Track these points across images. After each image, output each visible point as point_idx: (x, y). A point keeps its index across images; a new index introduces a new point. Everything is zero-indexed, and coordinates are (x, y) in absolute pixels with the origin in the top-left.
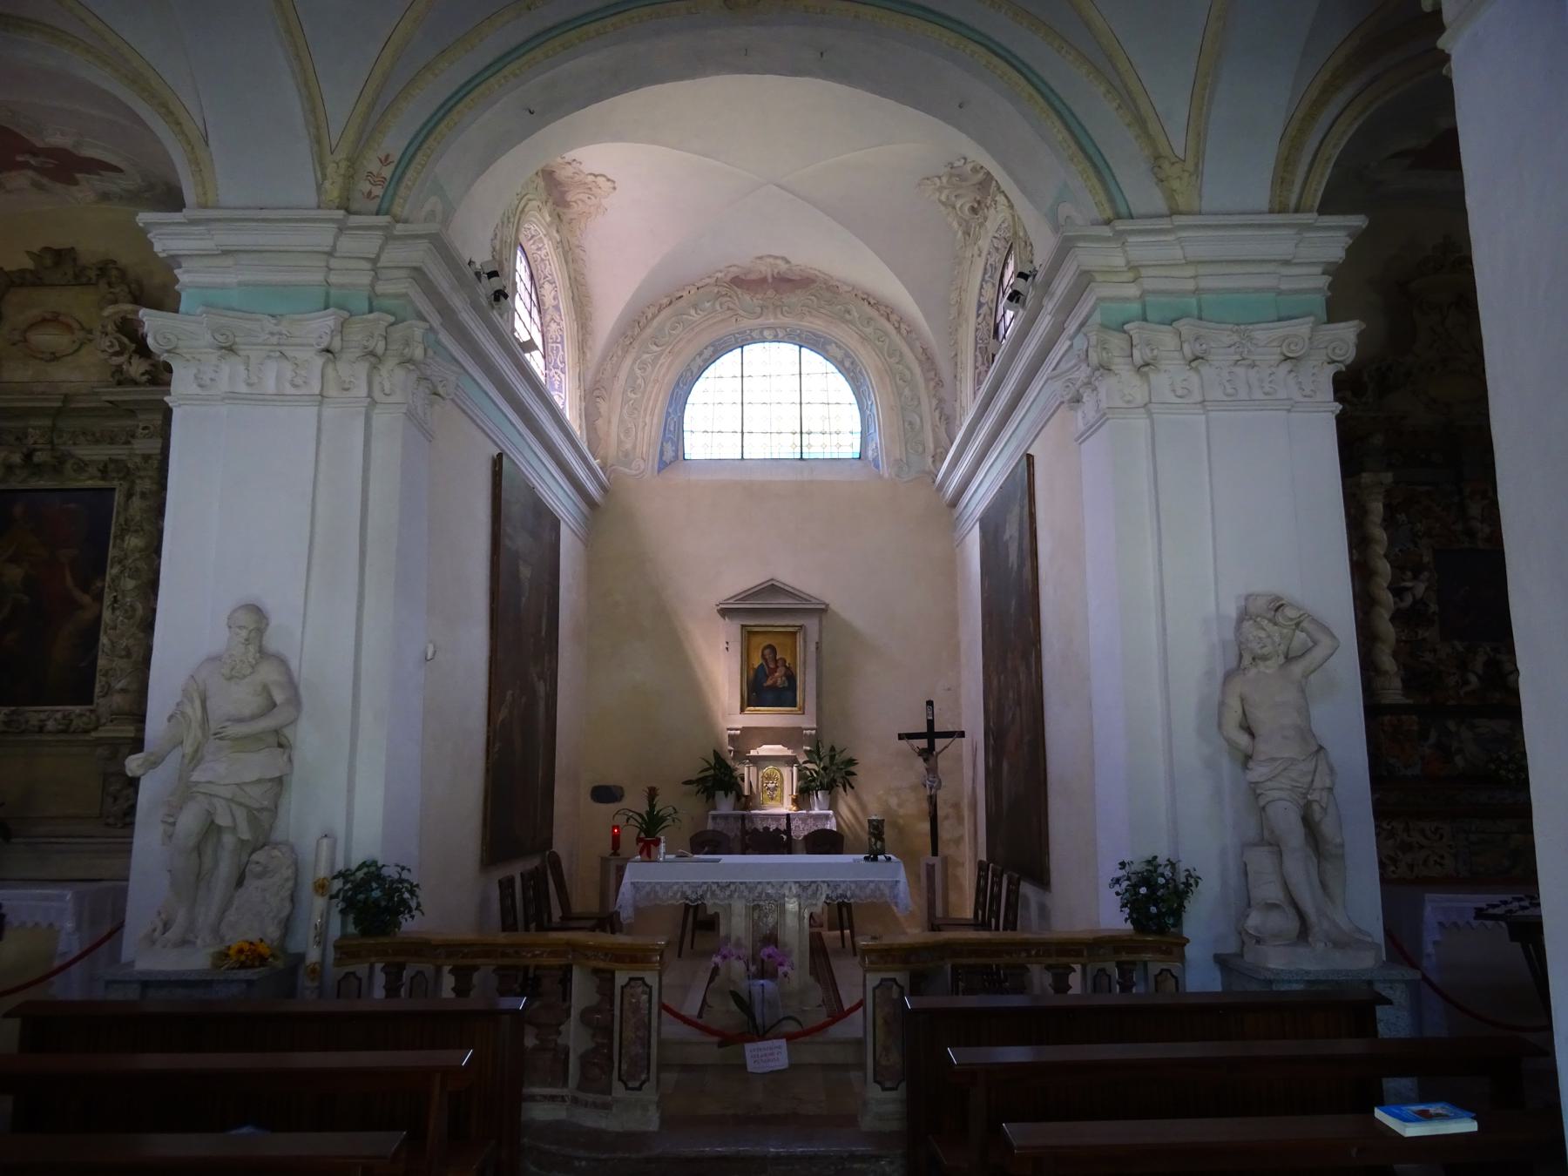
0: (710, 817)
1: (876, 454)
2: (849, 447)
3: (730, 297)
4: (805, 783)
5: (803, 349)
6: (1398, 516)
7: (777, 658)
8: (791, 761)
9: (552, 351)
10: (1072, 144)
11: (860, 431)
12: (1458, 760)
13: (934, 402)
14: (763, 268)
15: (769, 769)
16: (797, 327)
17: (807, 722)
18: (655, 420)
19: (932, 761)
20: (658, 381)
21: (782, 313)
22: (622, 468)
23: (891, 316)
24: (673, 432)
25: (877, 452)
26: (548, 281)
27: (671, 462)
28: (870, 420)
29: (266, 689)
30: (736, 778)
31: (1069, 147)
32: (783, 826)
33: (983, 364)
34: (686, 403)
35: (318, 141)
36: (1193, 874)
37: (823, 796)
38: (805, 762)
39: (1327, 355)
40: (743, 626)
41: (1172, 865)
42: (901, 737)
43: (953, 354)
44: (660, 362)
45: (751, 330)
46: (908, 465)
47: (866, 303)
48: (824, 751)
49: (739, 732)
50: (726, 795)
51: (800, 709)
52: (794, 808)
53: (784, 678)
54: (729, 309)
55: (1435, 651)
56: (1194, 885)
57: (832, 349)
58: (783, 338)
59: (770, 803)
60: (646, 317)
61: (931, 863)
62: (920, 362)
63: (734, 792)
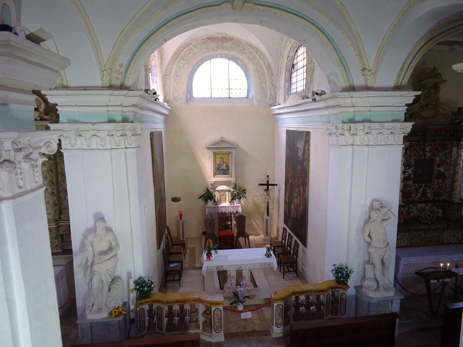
1: (252, 97)
2: (244, 94)
3: (207, 43)
6: (407, 151)
7: (224, 161)
10: (339, 60)
12: (412, 214)
13: (270, 81)
17: (232, 179)
18: (184, 86)
19: (268, 192)
20: (185, 73)
21: (224, 50)
22: (175, 102)
23: (258, 51)
24: (190, 89)
25: (253, 96)
27: (189, 99)
28: (250, 86)
29: (109, 241)
31: (338, 62)
35: (100, 63)
36: (352, 271)
37: (237, 200)
39: (403, 131)
40: (214, 152)
41: (347, 267)
43: (278, 67)
44: (185, 67)
45: (213, 55)
46: (262, 101)
47: (250, 47)
48: (238, 188)
49: (213, 183)
51: (230, 176)
53: (226, 167)
55: (411, 187)
56: (352, 273)
57: (239, 61)
58: (223, 57)
61: (267, 219)
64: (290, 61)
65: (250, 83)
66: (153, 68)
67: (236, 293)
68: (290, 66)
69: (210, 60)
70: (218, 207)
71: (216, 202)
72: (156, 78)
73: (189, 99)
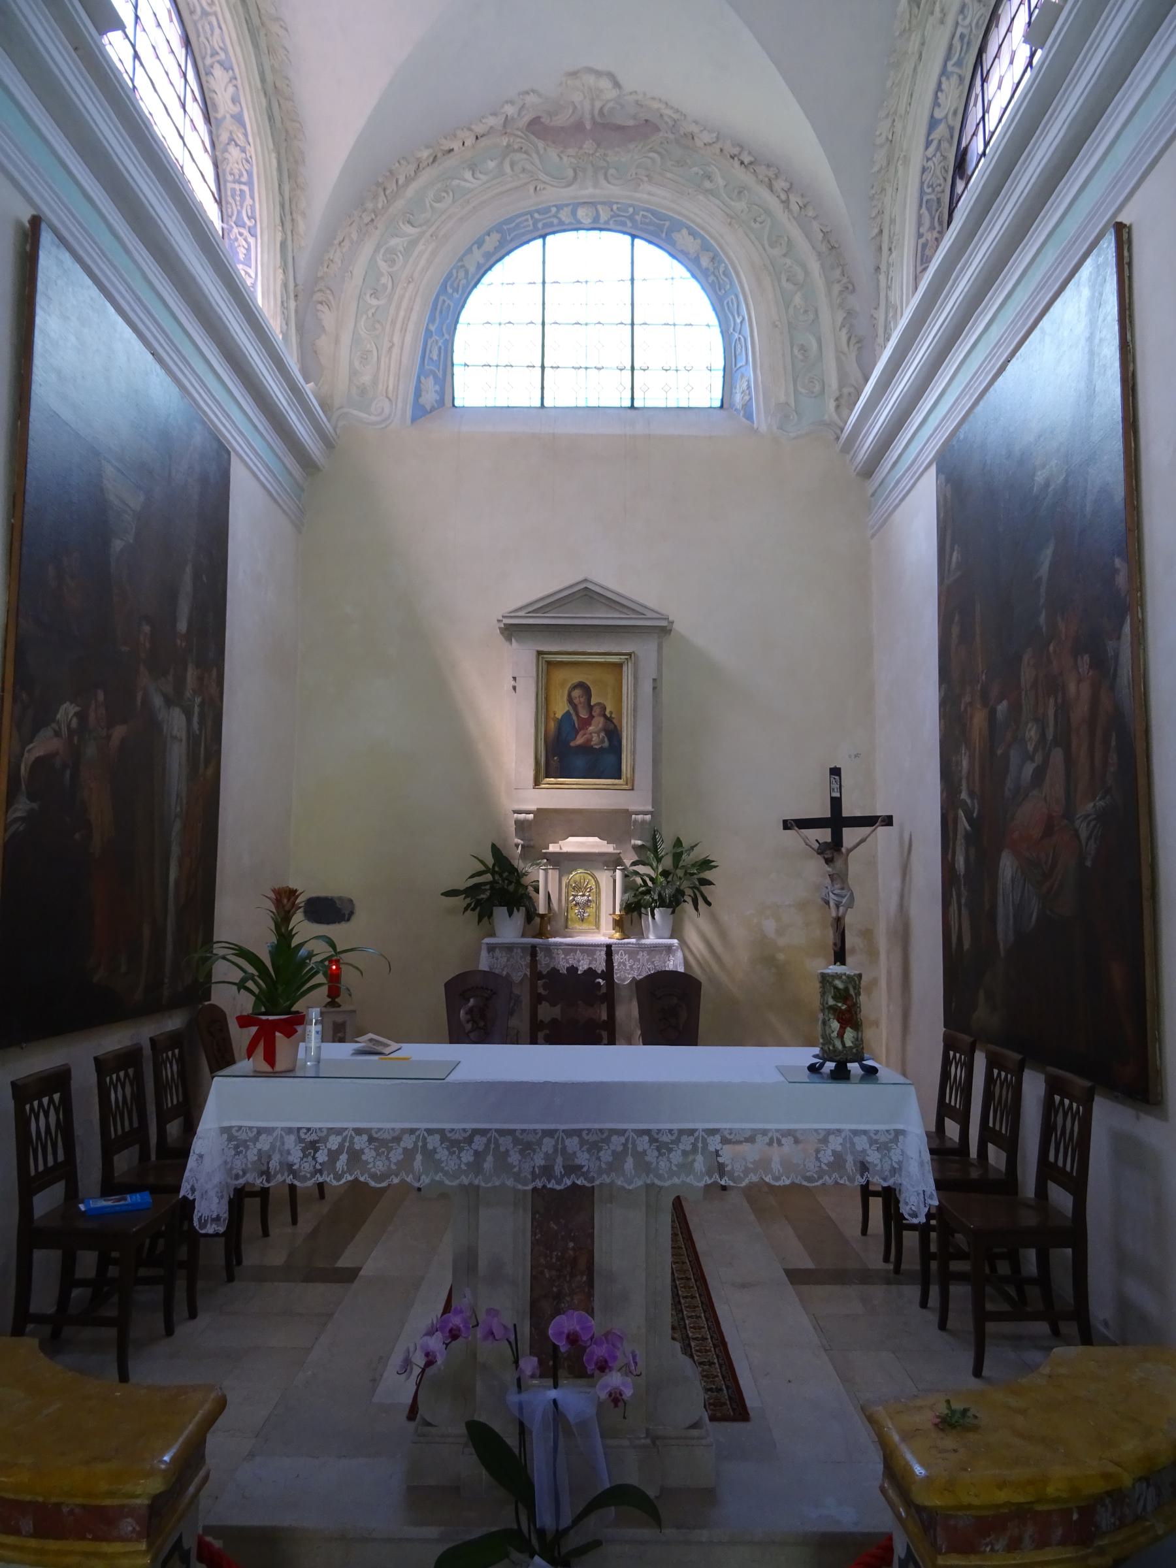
0: (484, 947)
1: (747, 398)
3: (526, 152)
4: (635, 896)
5: (637, 241)
7: (592, 704)
8: (613, 862)
9: (233, 196)
11: (722, 366)
13: (840, 316)
14: (577, 97)
15: (577, 875)
16: (629, 202)
18: (408, 339)
19: (839, 863)
21: (606, 178)
22: (356, 412)
25: (750, 394)
26: (219, 62)
27: (433, 409)
28: (739, 346)
30: (526, 887)
32: (600, 966)
33: (932, 228)
34: (457, 322)
37: (662, 916)
38: (634, 864)
40: (540, 653)
42: (787, 825)
43: (876, 231)
45: (559, 208)
47: (736, 163)
48: (665, 848)
49: (531, 816)
50: (510, 914)
52: (617, 935)
53: (602, 734)
54: (524, 170)
57: (683, 239)
58: (607, 222)
59: (579, 926)
60: (397, 182)
62: (819, 254)
63: (523, 909)
64: (945, 145)
65: (736, 335)
66: (233, 190)
67: (512, 1441)
68: (945, 179)
69: (544, 237)
70: (548, 949)
71: (542, 916)
72: (245, 240)
73: (428, 408)
